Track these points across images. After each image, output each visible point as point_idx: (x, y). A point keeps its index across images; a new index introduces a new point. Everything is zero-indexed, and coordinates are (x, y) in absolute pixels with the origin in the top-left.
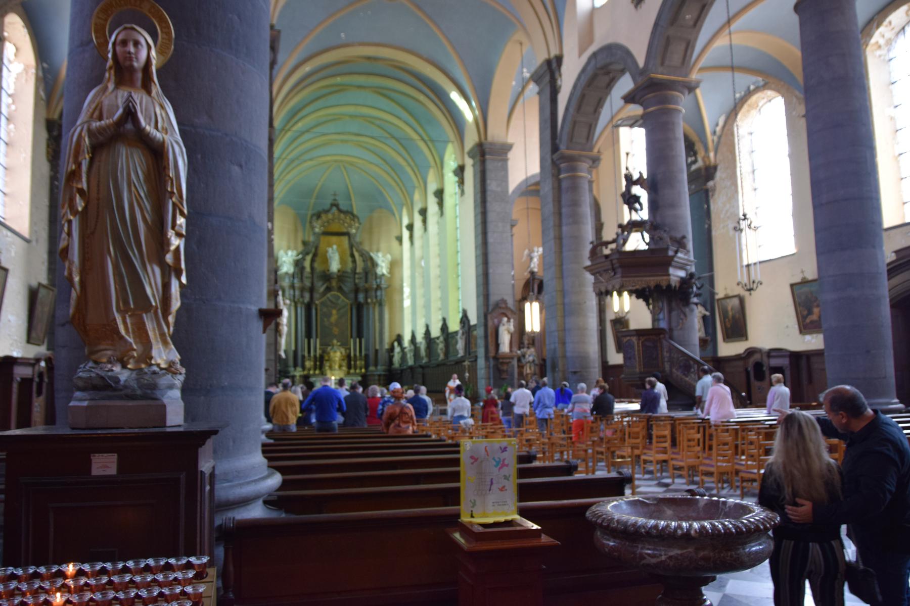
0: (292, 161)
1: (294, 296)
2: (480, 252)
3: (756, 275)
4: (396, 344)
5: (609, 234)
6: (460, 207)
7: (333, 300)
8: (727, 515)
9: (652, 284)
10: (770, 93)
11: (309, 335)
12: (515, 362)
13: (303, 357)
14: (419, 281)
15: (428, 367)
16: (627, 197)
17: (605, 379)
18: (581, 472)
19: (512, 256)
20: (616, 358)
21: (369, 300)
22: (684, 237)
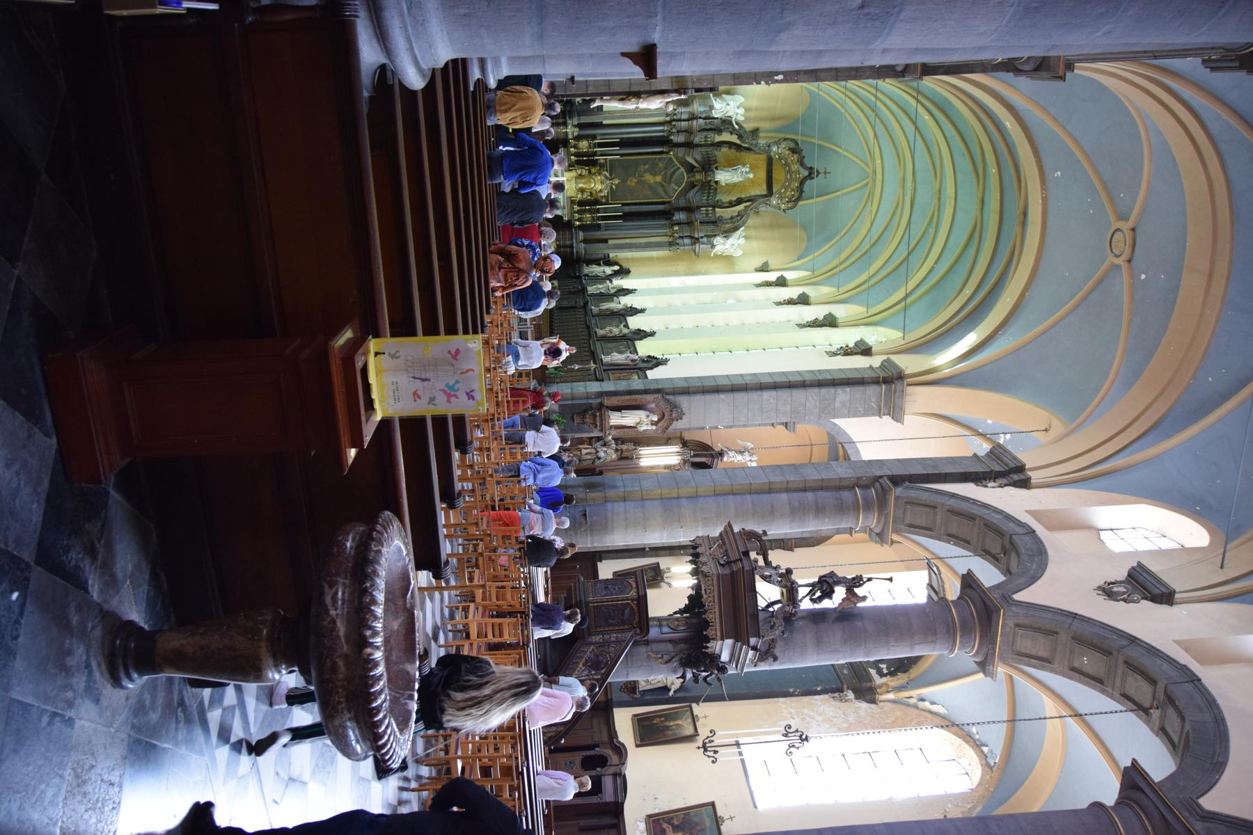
0: (873, 109)
1: (680, 120)
2: (748, 380)
4: (616, 268)
5: (778, 558)
6: (812, 353)
7: (675, 177)
8: (394, 700)
9: (709, 616)
10: (977, 773)
11: (624, 143)
12: (596, 434)
13: (594, 137)
14: (706, 297)
15: (586, 314)
16: (830, 580)
17: (577, 556)
18: (447, 517)
19: (744, 426)
20: (606, 570)
21: (676, 228)
22: (775, 659)
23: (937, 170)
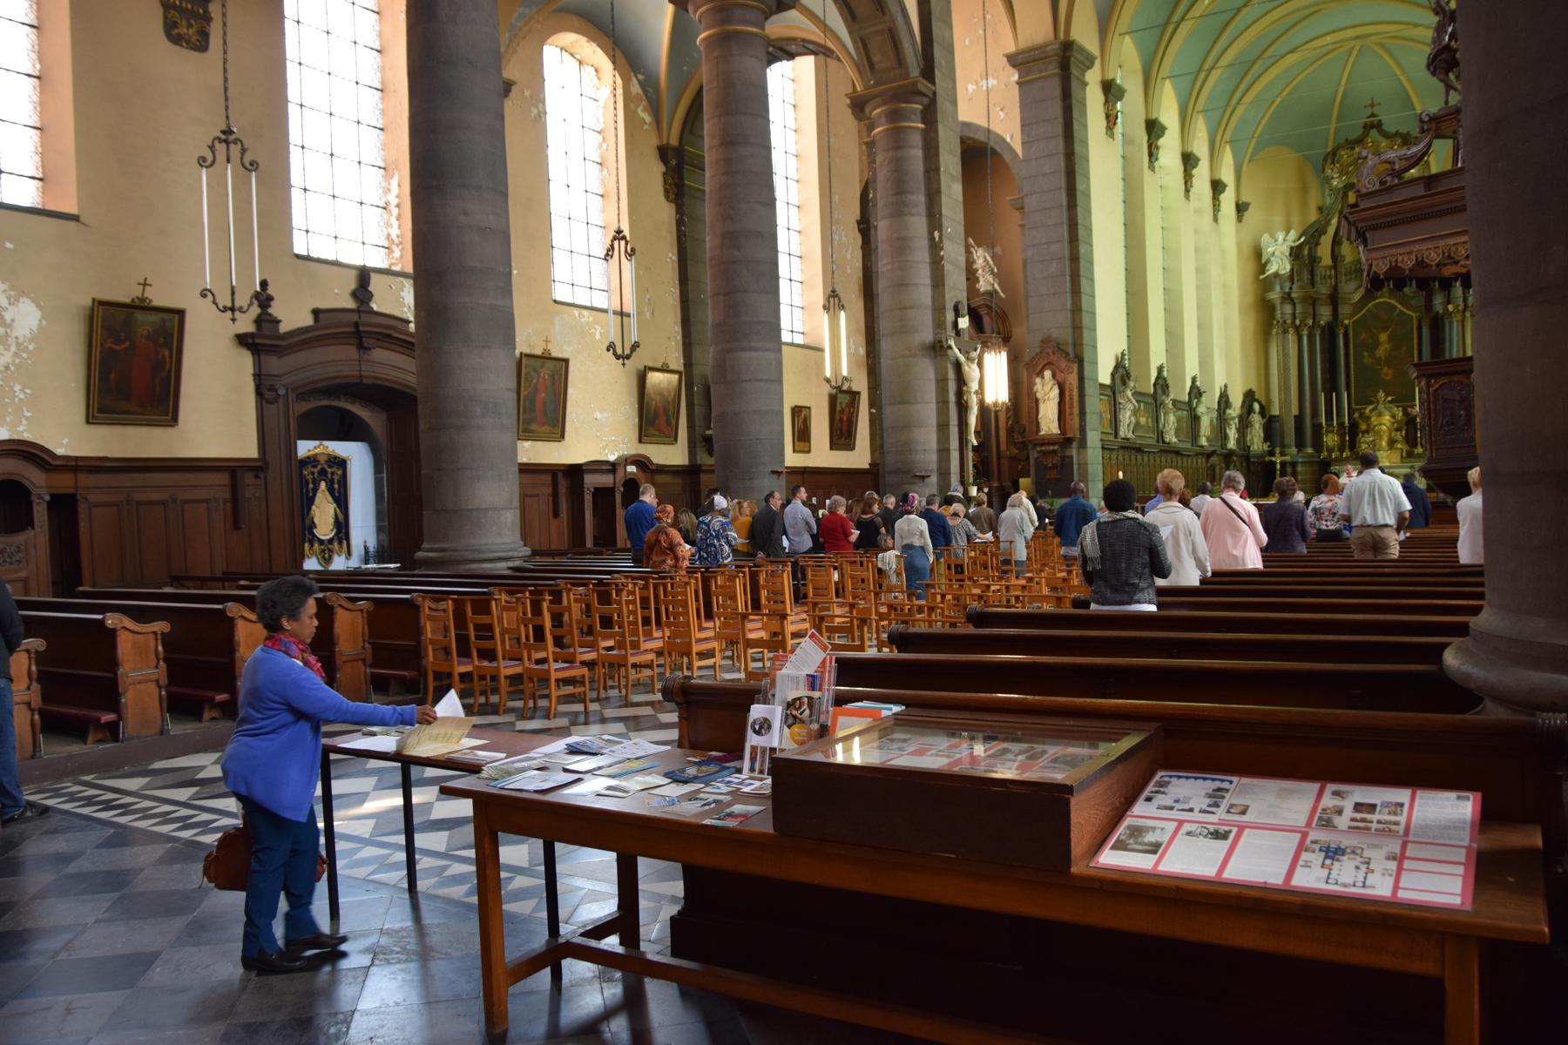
3: (1205, 361)
9: (1408, 263)
11: (1331, 385)
13: (1317, 428)
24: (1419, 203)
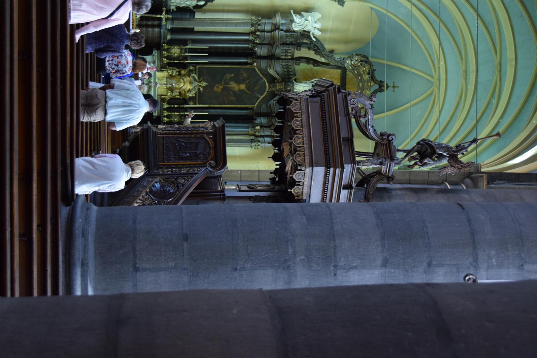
9: (295, 124)
11: (212, 53)
13: (185, 42)
23: (497, 47)
24: (335, 133)
